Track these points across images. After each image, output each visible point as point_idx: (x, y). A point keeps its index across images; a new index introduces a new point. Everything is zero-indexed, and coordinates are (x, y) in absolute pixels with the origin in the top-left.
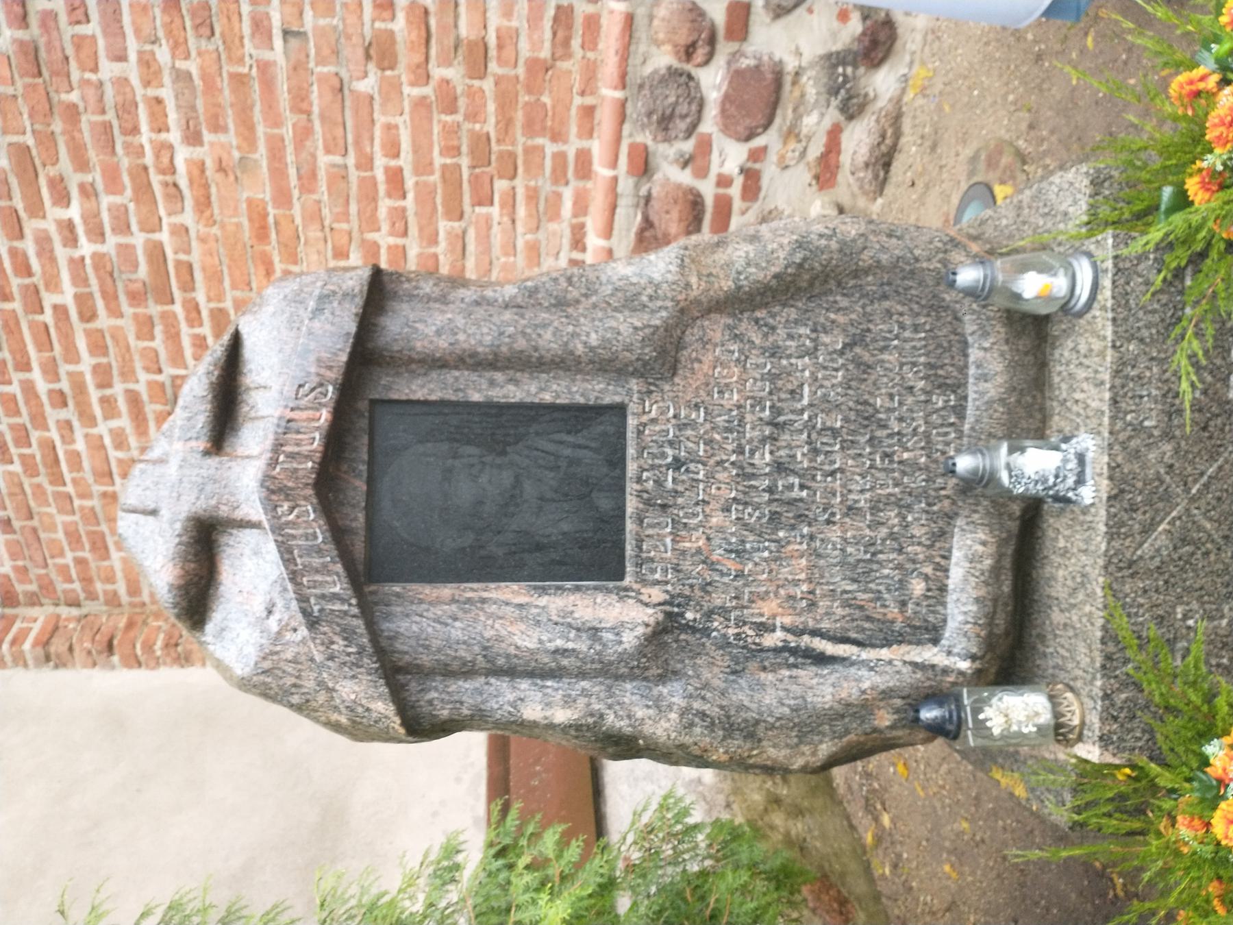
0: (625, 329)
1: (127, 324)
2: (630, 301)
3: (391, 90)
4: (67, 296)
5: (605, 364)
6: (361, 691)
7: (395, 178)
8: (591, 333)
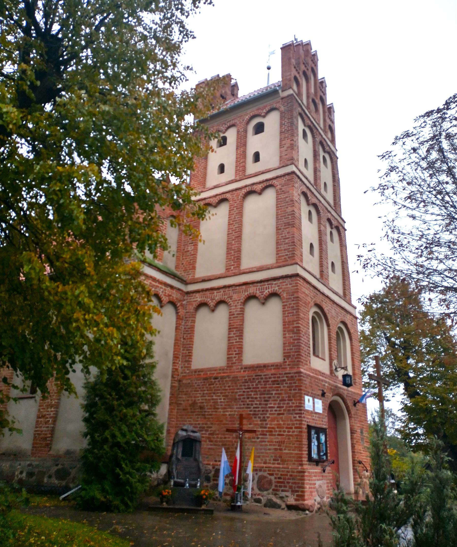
0: (197, 457)
1: (211, 404)
2: (199, 457)
3: (233, 438)
4: (214, 397)
5: (195, 456)
6: (177, 440)
7: (225, 438)
8: (197, 455)
